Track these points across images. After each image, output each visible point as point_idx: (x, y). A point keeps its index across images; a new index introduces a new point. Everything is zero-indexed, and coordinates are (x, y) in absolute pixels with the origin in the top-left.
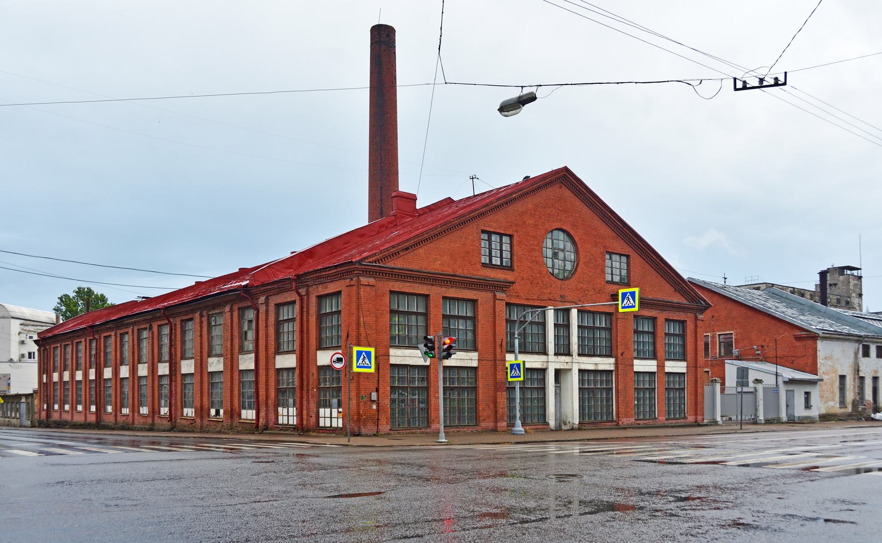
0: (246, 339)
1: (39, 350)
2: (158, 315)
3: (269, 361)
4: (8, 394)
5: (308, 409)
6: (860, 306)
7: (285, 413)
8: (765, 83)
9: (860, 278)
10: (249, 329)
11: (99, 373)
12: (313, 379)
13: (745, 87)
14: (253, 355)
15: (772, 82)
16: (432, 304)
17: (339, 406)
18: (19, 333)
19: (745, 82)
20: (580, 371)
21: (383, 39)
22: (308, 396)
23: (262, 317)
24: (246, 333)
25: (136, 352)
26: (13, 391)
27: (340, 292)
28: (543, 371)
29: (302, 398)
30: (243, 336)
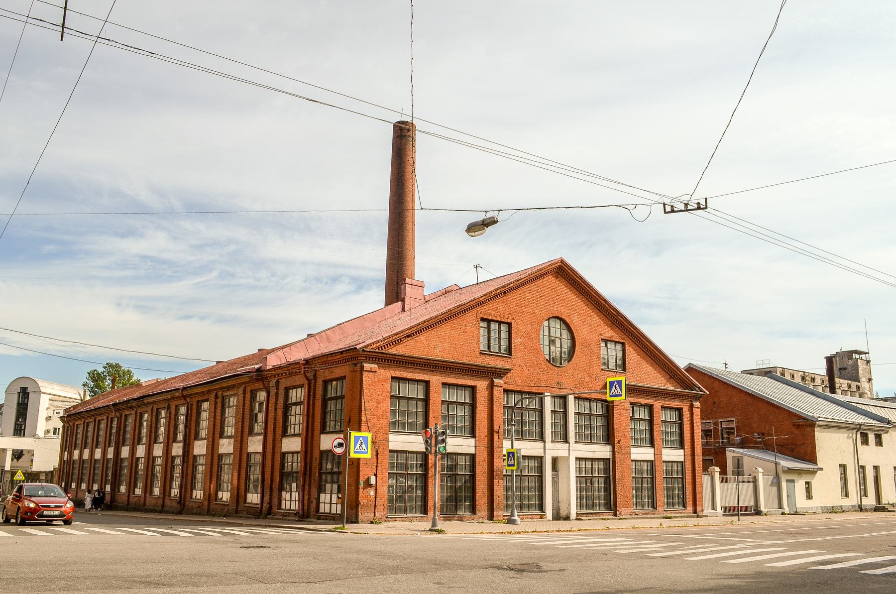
0: (256, 421)
1: (64, 427)
2: (177, 395)
3: (276, 444)
4: (30, 470)
5: (309, 495)
6: (871, 390)
7: (288, 498)
8: (689, 207)
9: (868, 362)
10: (259, 411)
11: (117, 452)
12: (316, 464)
13: (673, 211)
14: (261, 437)
15: (696, 206)
16: (432, 389)
17: (339, 491)
18: (48, 408)
19: (672, 206)
21: (403, 134)
22: (310, 481)
23: (272, 400)
24: (257, 415)
25: (153, 431)
26: (35, 468)
27: (345, 377)
28: (540, 459)
29: (304, 482)
30: (254, 418)
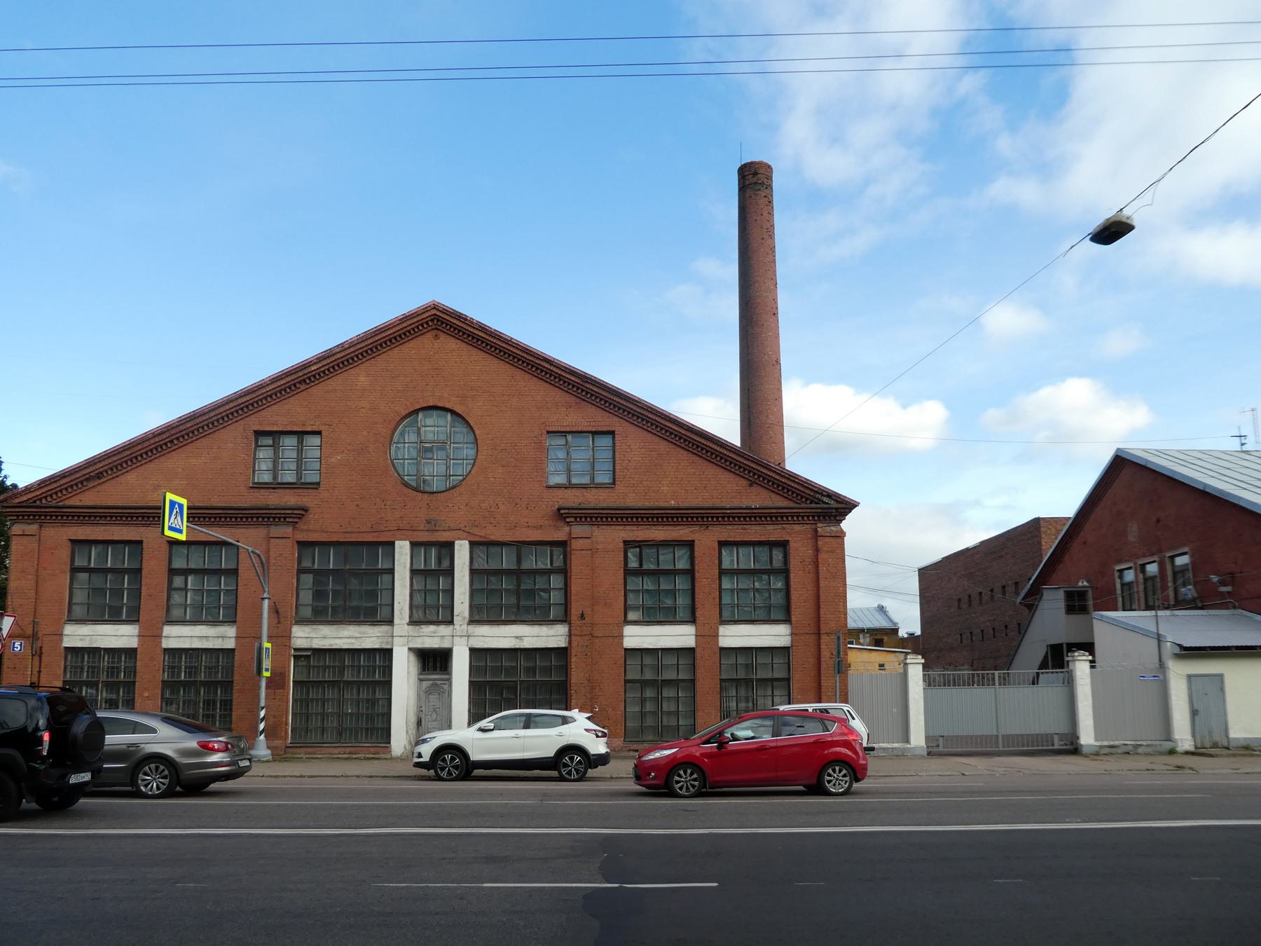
20: (473, 651)
